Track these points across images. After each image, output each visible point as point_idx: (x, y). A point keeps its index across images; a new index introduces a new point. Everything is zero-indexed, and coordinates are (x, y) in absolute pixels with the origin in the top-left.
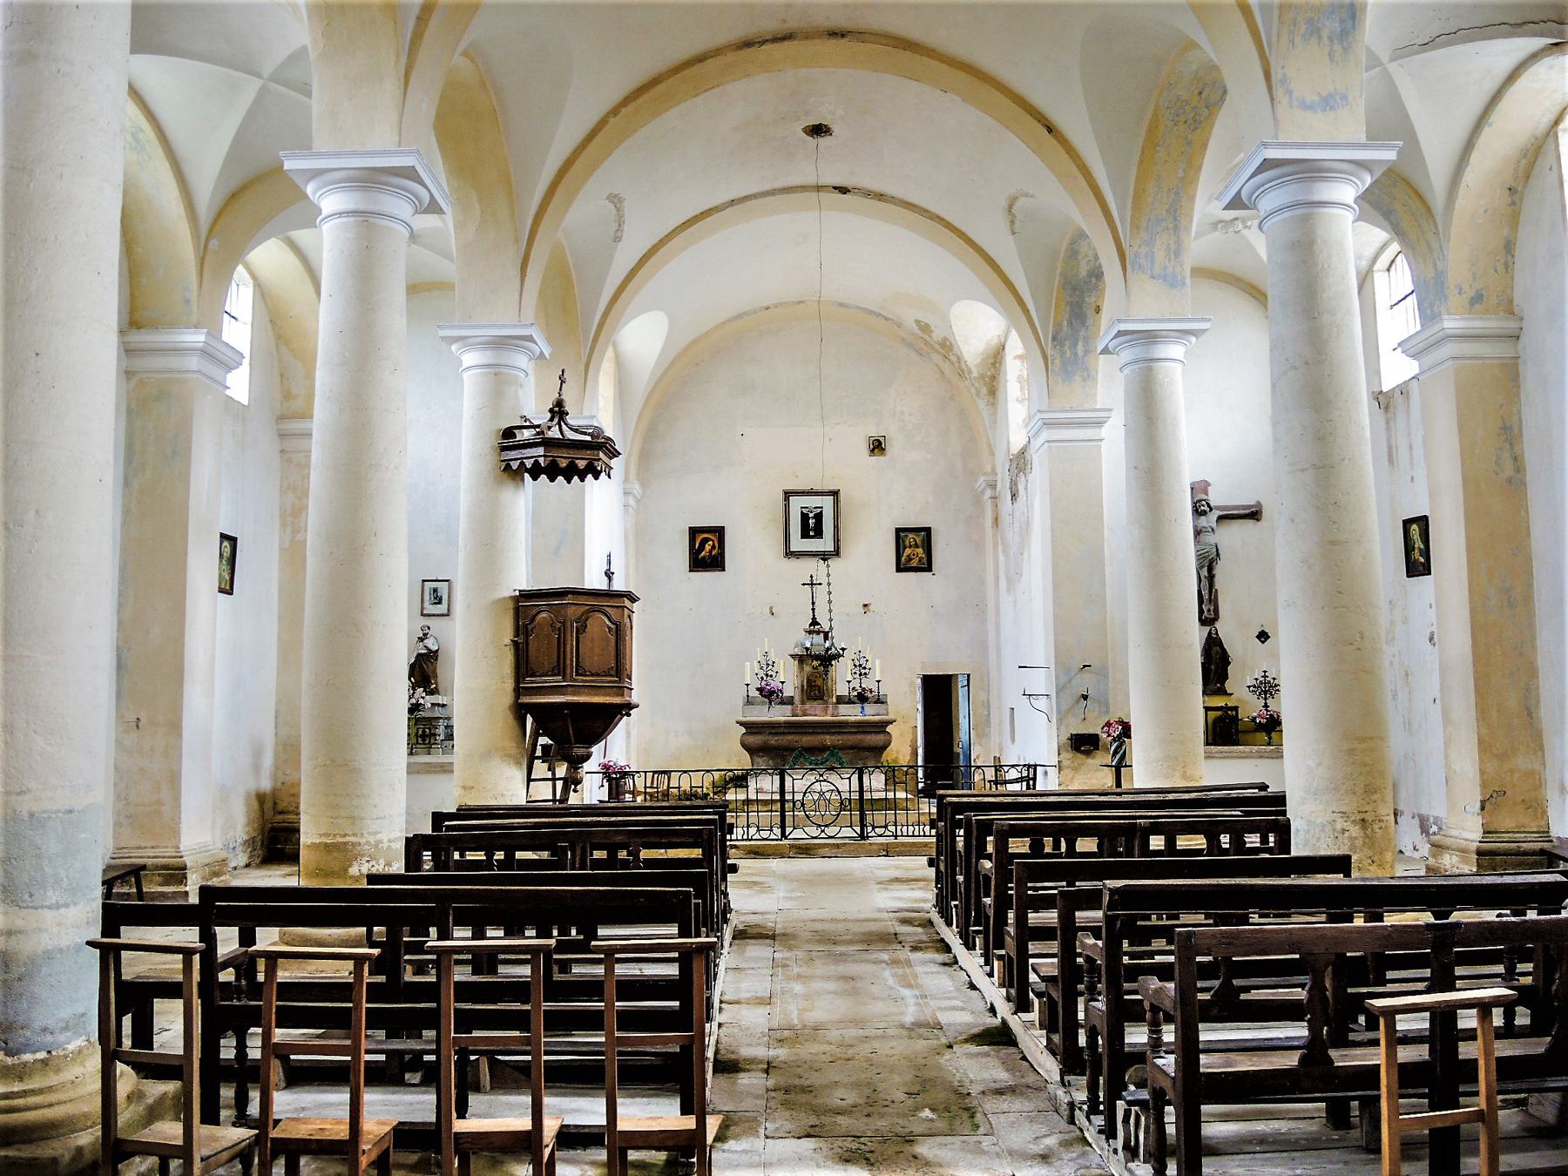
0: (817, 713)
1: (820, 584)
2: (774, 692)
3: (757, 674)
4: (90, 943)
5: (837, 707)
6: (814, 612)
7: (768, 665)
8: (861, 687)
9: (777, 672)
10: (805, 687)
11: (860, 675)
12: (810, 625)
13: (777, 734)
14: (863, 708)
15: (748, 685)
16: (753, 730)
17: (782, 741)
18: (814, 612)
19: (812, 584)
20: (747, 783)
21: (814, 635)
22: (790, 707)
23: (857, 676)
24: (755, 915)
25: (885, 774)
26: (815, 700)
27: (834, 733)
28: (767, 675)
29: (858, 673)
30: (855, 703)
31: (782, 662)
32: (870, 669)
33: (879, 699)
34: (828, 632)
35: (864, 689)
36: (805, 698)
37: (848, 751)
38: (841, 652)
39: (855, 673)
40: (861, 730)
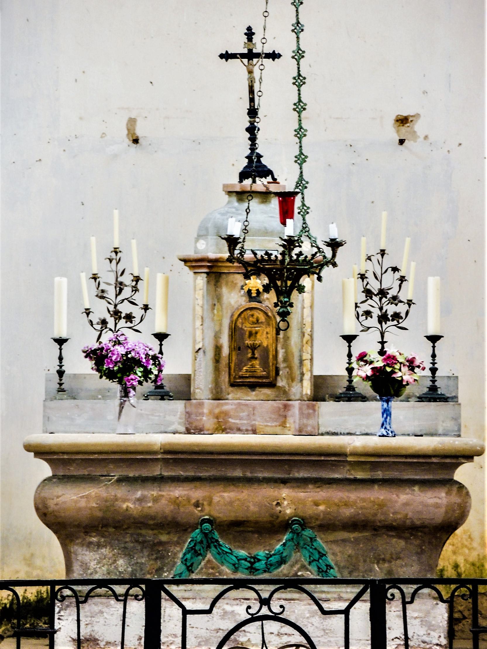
0: (258, 423)
1: (274, 56)
2: (137, 362)
3: (88, 312)
4: (378, 342)
5: (313, 408)
6: (253, 139)
7: (120, 287)
8: (382, 352)
9: (146, 308)
10: (225, 351)
11: (383, 318)
12: (243, 176)
13: (144, 480)
14: (387, 413)
15: (60, 342)
16: (73, 471)
17: (156, 500)
18: (253, 139)
19: (250, 55)
20: (51, 623)
21: (255, 204)
22: (179, 406)
23: (373, 322)
24: (247, 597)
25: (450, 602)
26: (253, 386)
27: (304, 482)
28: (117, 314)
29: (376, 312)
30: (364, 399)
31: (160, 278)
32: (410, 303)
33: (433, 388)
34: (294, 194)
35: (391, 360)
36: (225, 378)
37: (345, 535)
38: (328, 252)
39: (368, 314)
40: (379, 474)
